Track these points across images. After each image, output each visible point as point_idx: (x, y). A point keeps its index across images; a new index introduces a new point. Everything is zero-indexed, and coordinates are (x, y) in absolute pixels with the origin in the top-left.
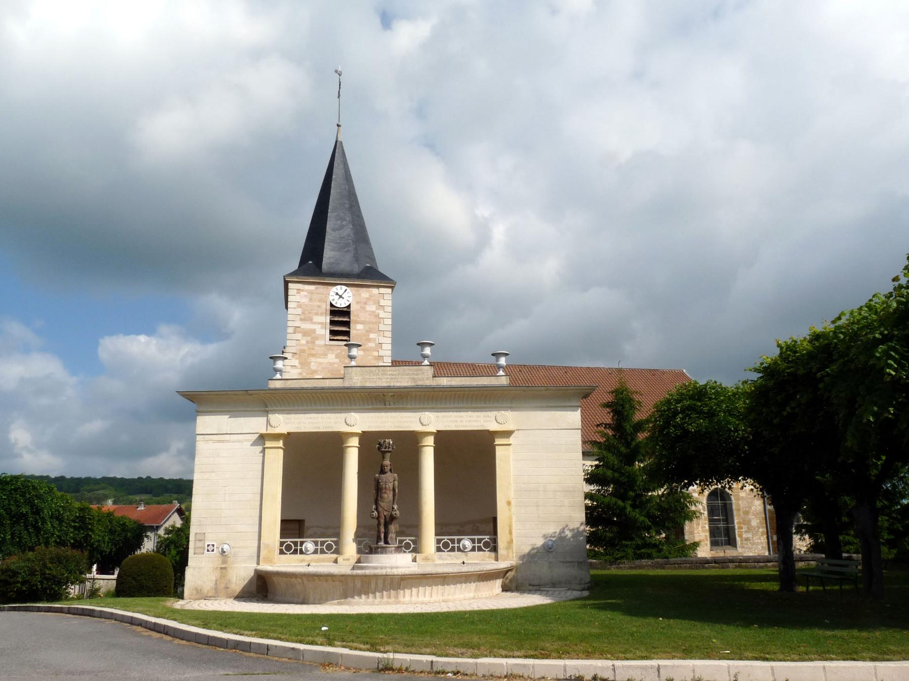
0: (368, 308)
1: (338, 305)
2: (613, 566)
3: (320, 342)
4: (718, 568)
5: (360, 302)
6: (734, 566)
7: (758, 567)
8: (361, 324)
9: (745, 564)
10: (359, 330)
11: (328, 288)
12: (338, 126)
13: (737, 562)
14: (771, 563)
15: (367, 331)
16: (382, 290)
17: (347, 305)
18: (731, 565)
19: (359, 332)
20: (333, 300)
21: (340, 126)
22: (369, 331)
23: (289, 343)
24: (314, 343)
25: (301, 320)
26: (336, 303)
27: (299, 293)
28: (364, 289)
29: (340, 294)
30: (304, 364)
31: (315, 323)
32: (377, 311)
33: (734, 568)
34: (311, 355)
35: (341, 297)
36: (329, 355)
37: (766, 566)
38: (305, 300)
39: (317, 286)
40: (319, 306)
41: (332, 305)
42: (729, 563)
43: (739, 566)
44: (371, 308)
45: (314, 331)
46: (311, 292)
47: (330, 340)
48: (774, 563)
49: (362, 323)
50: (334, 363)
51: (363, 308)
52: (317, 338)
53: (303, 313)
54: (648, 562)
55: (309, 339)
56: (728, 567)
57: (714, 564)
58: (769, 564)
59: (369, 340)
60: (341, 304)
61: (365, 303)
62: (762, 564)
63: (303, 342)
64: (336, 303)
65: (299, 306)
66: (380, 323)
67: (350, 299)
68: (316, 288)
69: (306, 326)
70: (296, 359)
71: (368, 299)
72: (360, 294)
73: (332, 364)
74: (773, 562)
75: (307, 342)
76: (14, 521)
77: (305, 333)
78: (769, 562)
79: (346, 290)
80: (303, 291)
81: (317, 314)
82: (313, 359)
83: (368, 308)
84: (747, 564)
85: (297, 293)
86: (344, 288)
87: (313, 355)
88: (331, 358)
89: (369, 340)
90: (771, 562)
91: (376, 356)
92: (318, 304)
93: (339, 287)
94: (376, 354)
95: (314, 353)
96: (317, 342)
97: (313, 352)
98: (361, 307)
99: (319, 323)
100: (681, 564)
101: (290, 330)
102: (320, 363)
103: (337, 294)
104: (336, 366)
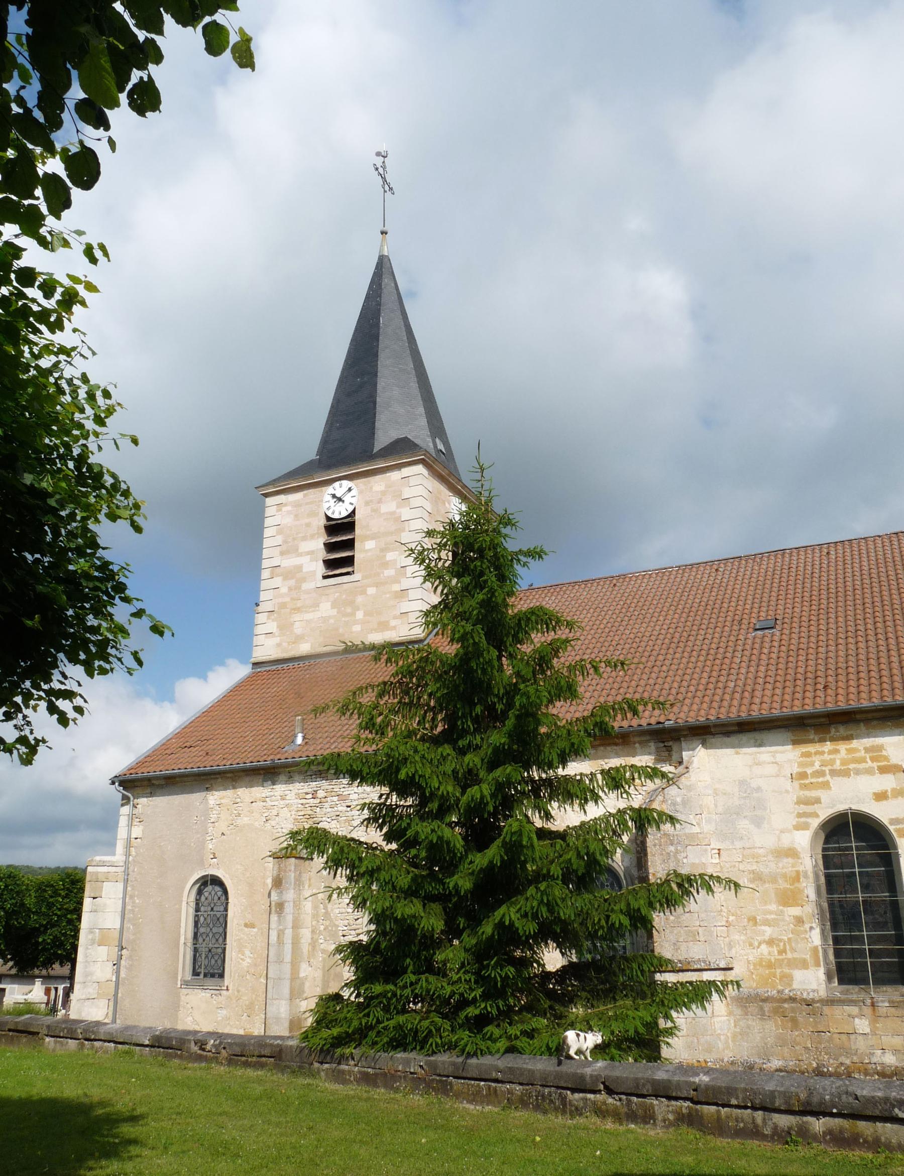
0: (384, 508)
1: (336, 516)
2: (326, 1066)
3: (308, 586)
4: (617, 1117)
5: (371, 501)
6: (671, 1117)
7: (767, 1131)
8: (372, 539)
9: (713, 1108)
10: (370, 550)
11: (322, 491)
12: (384, 233)
13: (685, 1099)
14: (823, 1120)
15: (382, 550)
16: (406, 471)
17: (350, 510)
18: (660, 1106)
19: (369, 554)
20: (328, 508)
21: (386, 233)
22: (385, 550)
23: (263, 596)
24: (300, 588)
25: (282, 553)
26: (333, 513)
27: (280, 510)
28: (378, 477)
29: (338, 495)
30: (286, 627)
31: (301, 555)
32: (398, 511)
33: (671, 1124)
34: (294, 609)
35: (340, 500)
36: (321, 605)
37: (804, 1133)
38: (288, 520)
39: (305, 492)
40: (308, 525)
41: (328, 519)
42: (657, 1096)
43: (690, 1115)
44: (389, 506)
45: (299, 568)
46: (297, 505)
47: (325, 577)
48: (838, 1121)
49: (373, 537)
50: (330, 617)
51: (374, 511)
52: (304, 580)
53: (285, 542)
54: (407, 1062)
55: (292, 582)
56: (647, 1117)
57: (602, 1097)
58: (818, 1125)
59: (385, 565)
60: (340, 512)
61: (380, 501)
62: (784, 1121)
63: (284, 590)
64: (333, 513)
65: (279, 532)
66: (404, 530)
67: (354, 500)
68: (305, 496)
69: (288, 562)
70: (273, 621)
71: (383, 493)
72: (371, 488)
73: (325, 619)
74: (832, 1115)
75: (290, 589)
76: (562, 930)
77: (288, 574)
78: (816, 1114)
79: (350, 490)
80: (286, 505)
81: (304, 539)
82: (297, 617)
83: (384, 508)
84: (724, 1111)
85: (278, 511)
86: (346, 484)
87: (298, 610)
88: (326, 609)
89: (385, 565)
90: (826, 1114)
91: (396, 592)
92: (307, 521)
93: (337, 484)
94: (396, 587)
95: (298, 605)
96: (305, 586)
97: (299, 604)
98: (373, 510)
99: (308, 553)
100: (496, 1081)
101: (265, 574)
102: (309, 622)
103: (334, 496)
104: (332, 621)
